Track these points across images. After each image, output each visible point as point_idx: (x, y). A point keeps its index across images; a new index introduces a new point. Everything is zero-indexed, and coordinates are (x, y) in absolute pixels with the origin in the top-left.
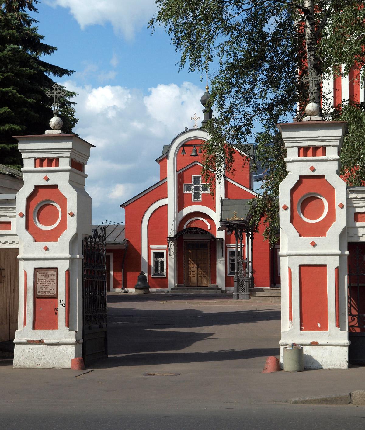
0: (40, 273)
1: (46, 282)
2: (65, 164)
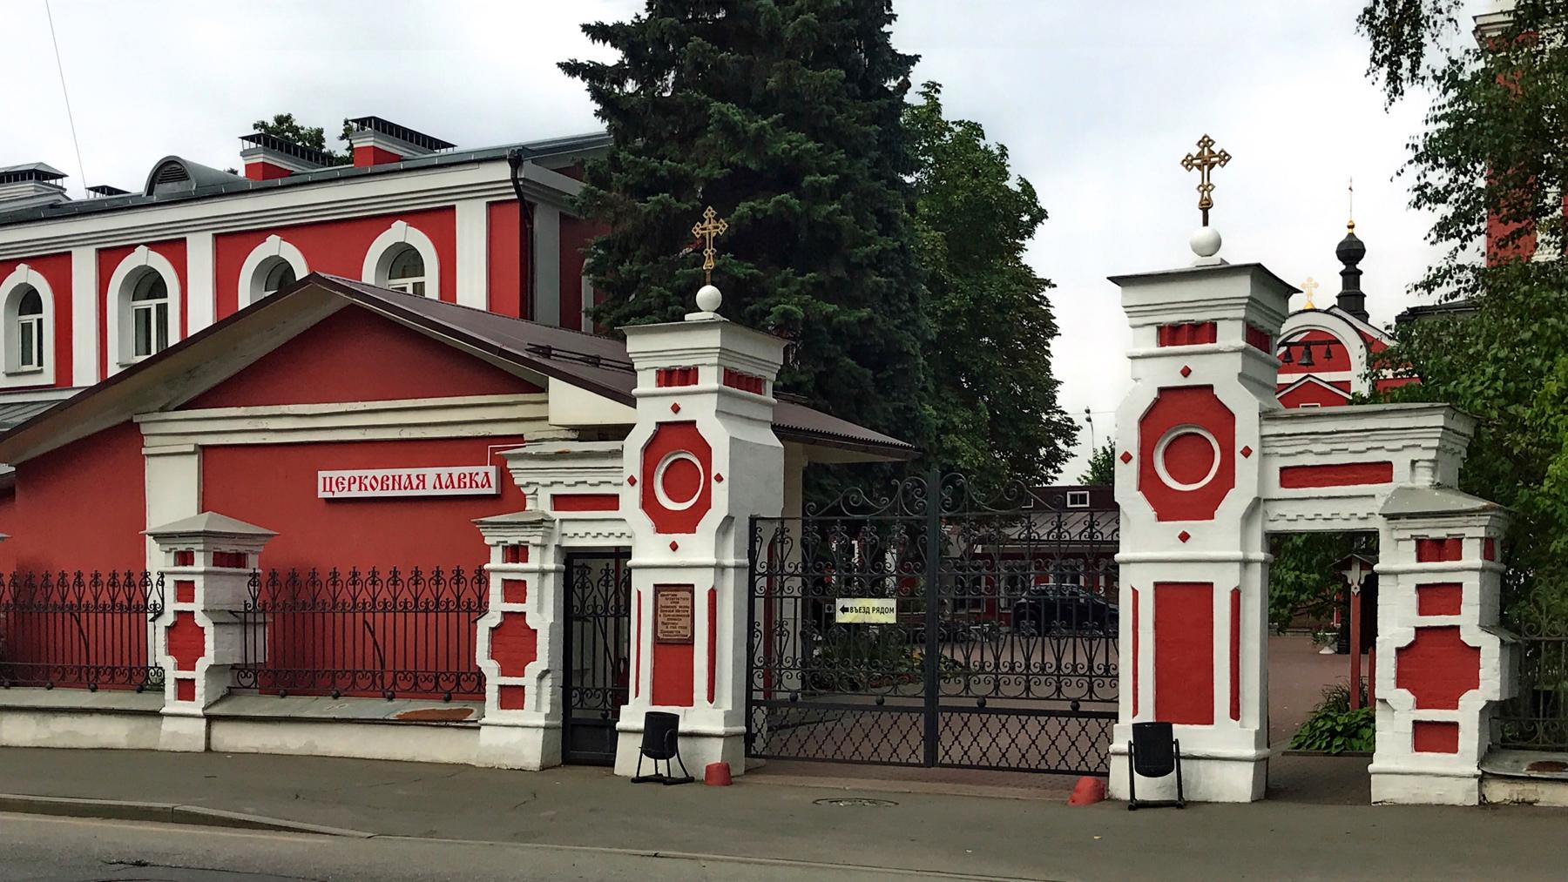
0: (662, 595)
1: (675, 613)
2: (1231, 336)
